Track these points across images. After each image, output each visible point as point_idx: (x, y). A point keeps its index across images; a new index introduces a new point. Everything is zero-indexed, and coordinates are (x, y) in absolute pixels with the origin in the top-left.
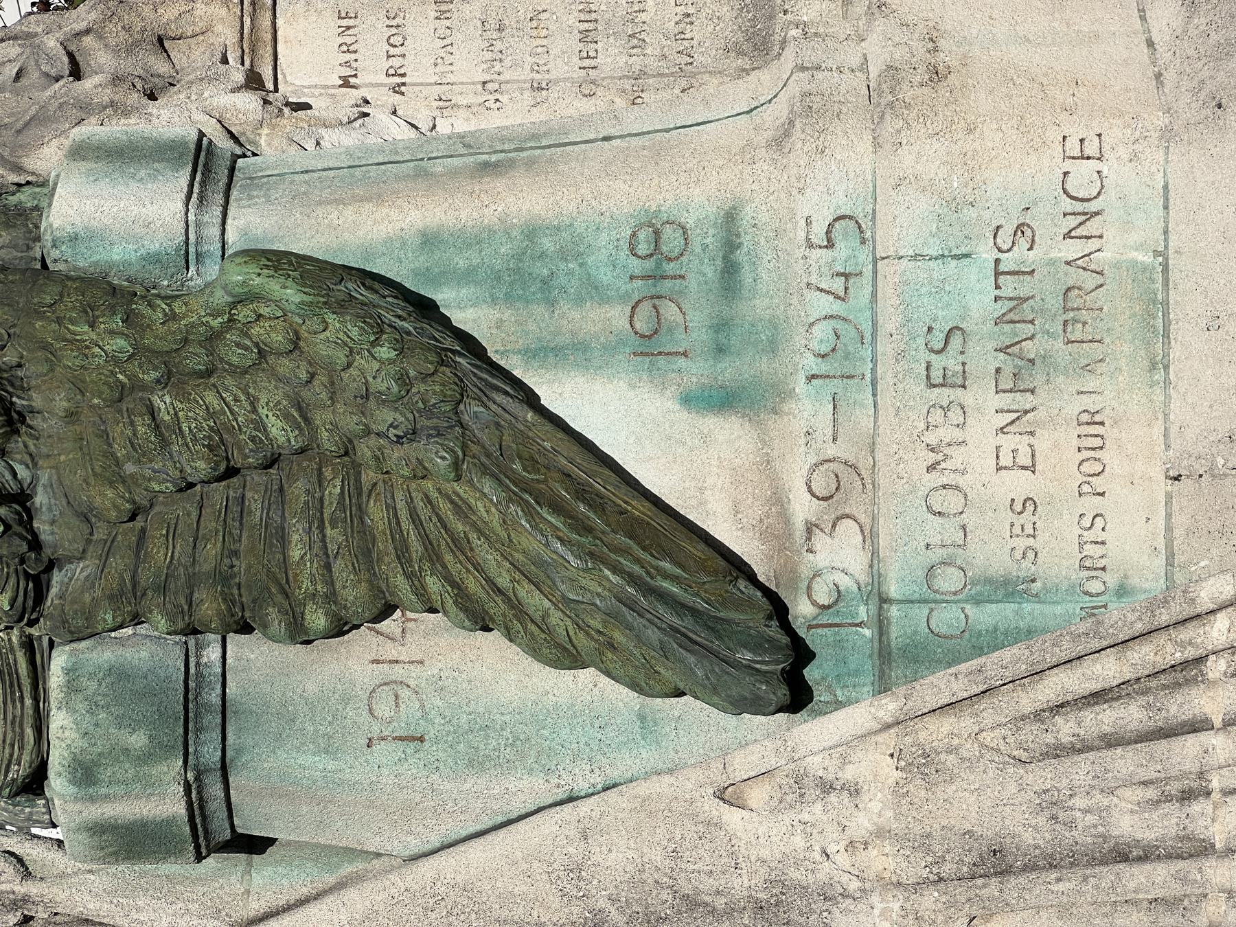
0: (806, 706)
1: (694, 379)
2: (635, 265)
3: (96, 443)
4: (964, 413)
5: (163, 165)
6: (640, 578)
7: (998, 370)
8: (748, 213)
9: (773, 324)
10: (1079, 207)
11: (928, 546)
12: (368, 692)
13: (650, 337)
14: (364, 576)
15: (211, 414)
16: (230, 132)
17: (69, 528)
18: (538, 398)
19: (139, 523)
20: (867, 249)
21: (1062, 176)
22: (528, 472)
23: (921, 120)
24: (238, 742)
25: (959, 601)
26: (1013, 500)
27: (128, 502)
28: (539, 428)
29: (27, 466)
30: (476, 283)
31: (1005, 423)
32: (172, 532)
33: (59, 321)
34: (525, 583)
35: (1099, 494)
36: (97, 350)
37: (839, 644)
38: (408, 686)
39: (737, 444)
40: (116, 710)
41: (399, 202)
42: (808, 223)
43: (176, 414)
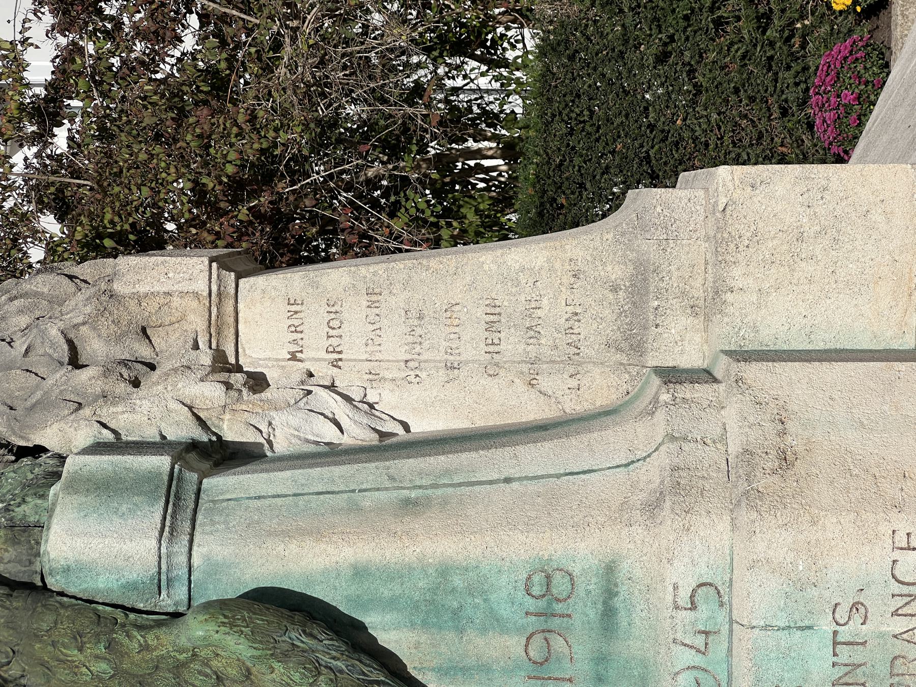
2: (531, 604)
5: (141, 498)
8: (624, 567)
10: (906, 590)
13: (541, 664)
16: (198, 418)
21: (892, 563)
23: (772, 513)
33: (54, 644)
36: (84, 670)
41: (334, 539)
42: (676, 587)
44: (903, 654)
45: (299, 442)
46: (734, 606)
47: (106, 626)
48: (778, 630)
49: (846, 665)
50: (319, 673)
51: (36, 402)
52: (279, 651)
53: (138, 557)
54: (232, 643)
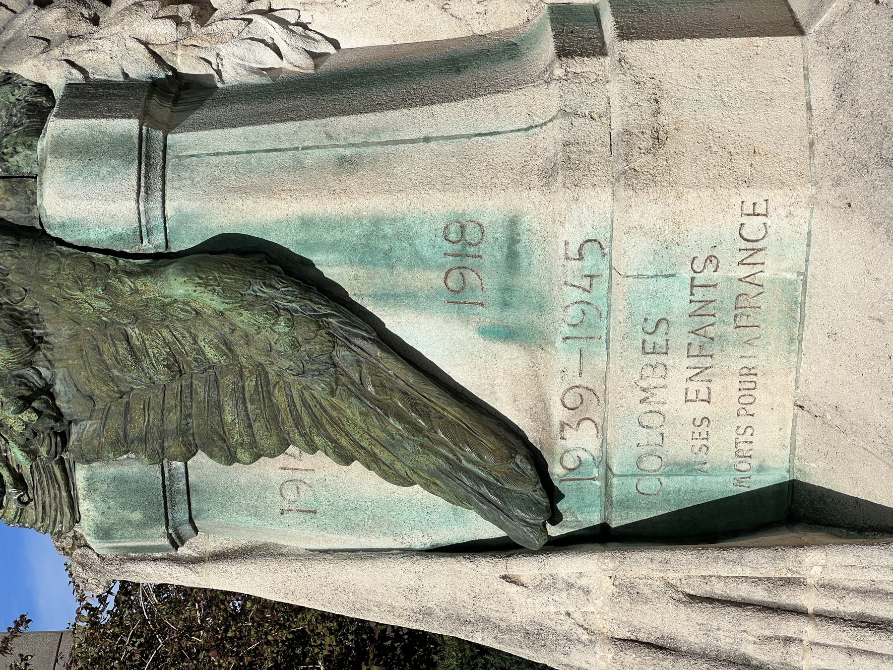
0: (558, 523)
1: (488, 320)
2: (448, 247)
3: (91, 353)
4: (666, 369)
5: (117, 162)
6: (453, 461)
7: (689, 344)
8: (525, 222)
9: (542, 296)
10: (750, 245)
11: (638, 445)
12: (279, 485)
13: (458, 292)
14: (274, 432)
15: (167, 344)
17: (79, 405)
18: (384, 324)
19: (125, 399)
20: (606, 260)
22: (380, 395)
23: (645, 190)
24: (198, 506)
25: (657, 475)
26: (695, 419)
27: (117, 393)
28: (386, 360)
29: (48, 369)
30: (339, 252)
31: (692, 375)
32: (147, 407)
34: (379, 446)
35: (750, 415)
36: (87, 305)
37: (579, 490)
38: (305, 483)
39: (516, 362)
40: (120, 500)
42: (566, 243)
43: (143, 341)
44: (746, 292)
45: (245, 73)
46: (614, 256)
47: (101, 272)
48: (648, 278)
49: (700, 302)
50: (279, 315)
51: (10, 39)
52: (245, 302)
53: (121, 214)
54: (207, 300)
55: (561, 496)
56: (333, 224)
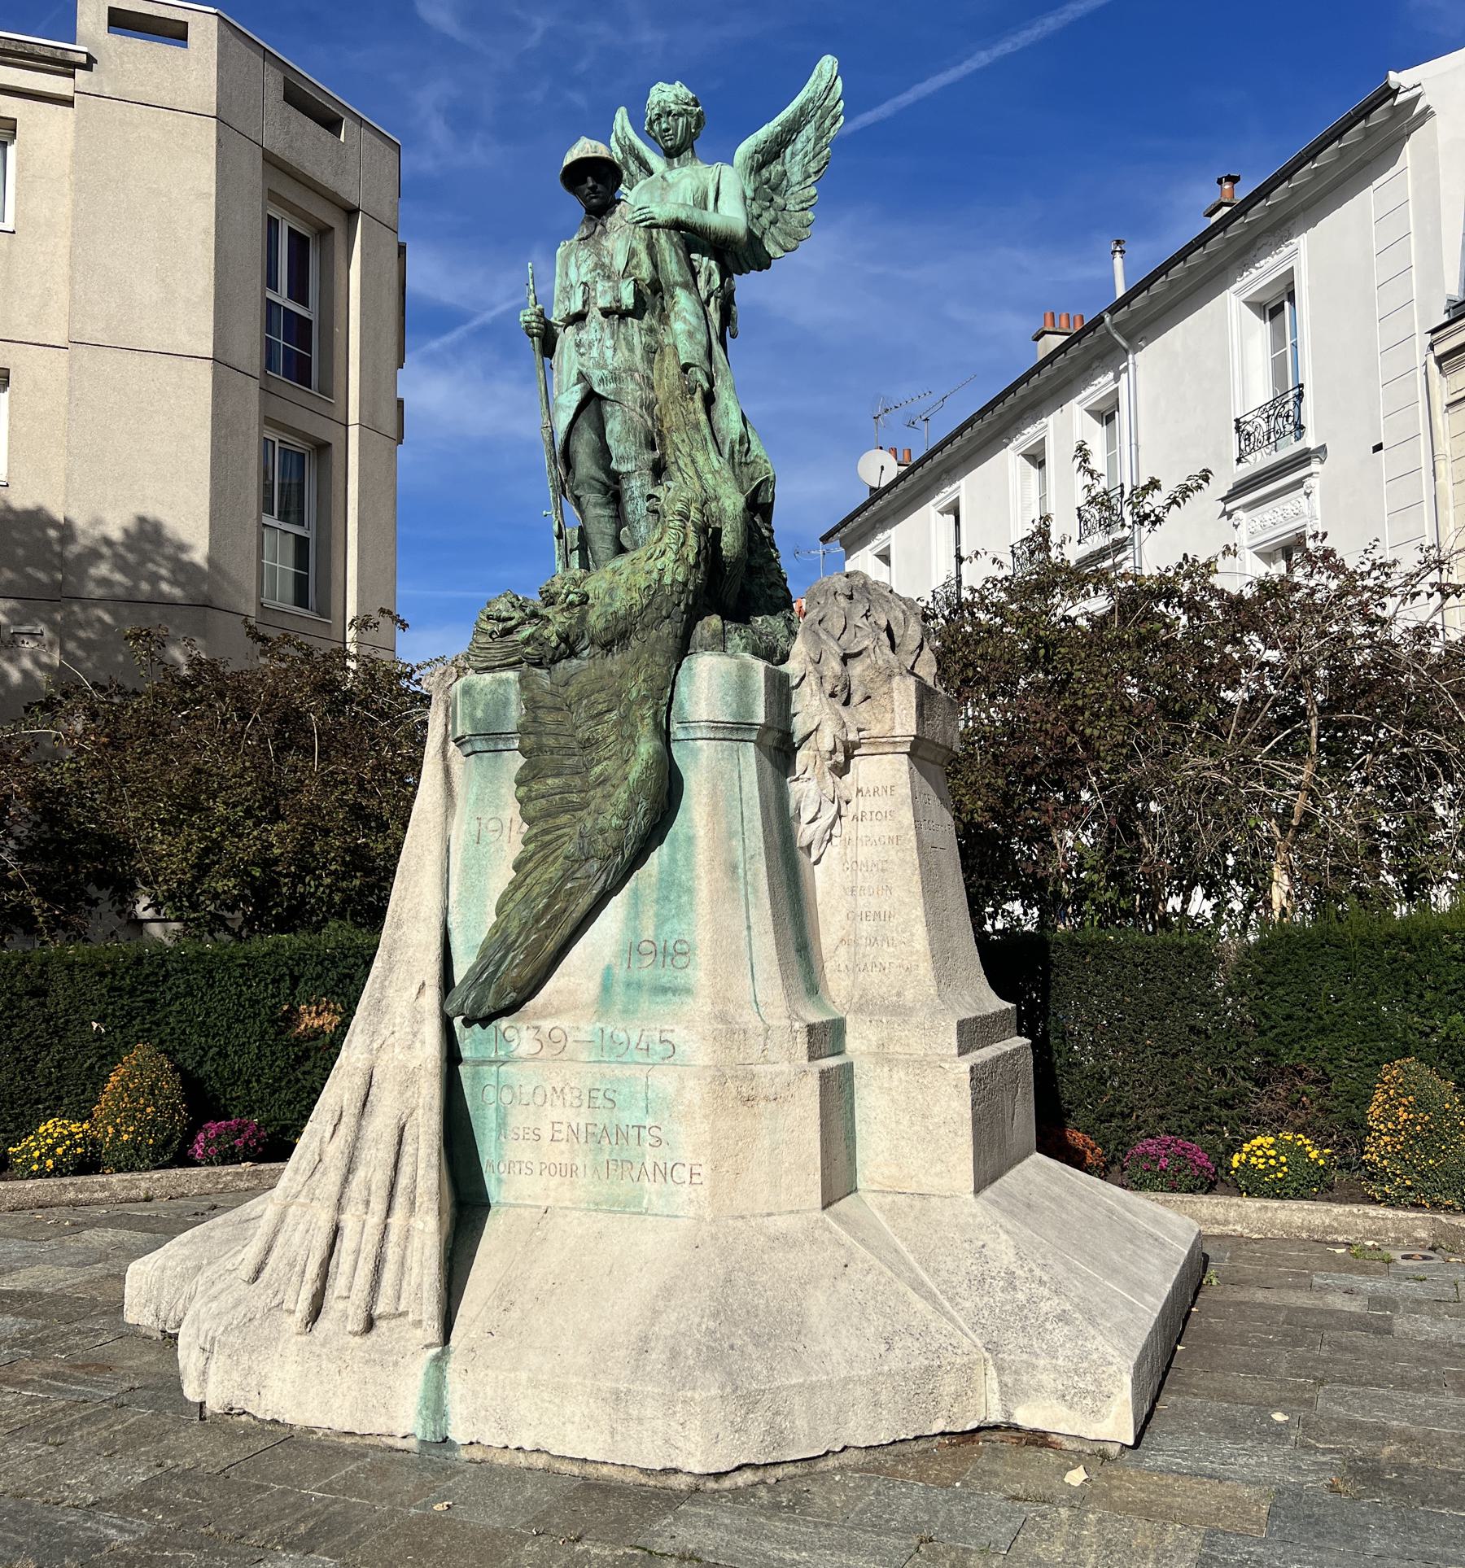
2: (671, 943)
3: (599, 685)
10: (669, 1171)
15: (604, 739)
19: (565, 708)
32: (559, 723)
33: (647, 665)
37: (489, 1041)
42: (672, 1031)
55: (484, 1028)
56: (689, 859)
